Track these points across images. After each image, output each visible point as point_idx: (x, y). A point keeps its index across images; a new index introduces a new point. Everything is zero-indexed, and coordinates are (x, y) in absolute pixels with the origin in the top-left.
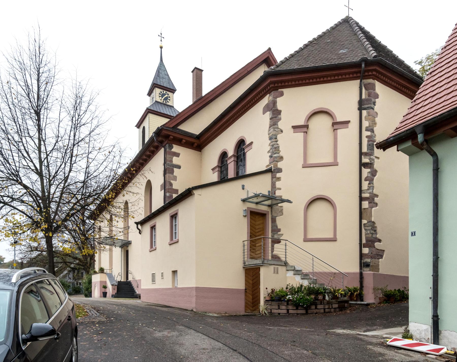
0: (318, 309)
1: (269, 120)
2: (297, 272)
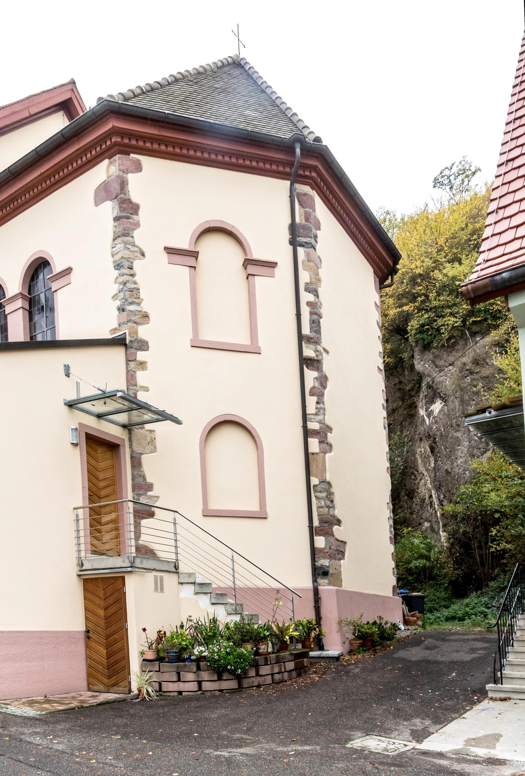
0: (261, 676)
1: (111, 223)
2: (203, 588)
